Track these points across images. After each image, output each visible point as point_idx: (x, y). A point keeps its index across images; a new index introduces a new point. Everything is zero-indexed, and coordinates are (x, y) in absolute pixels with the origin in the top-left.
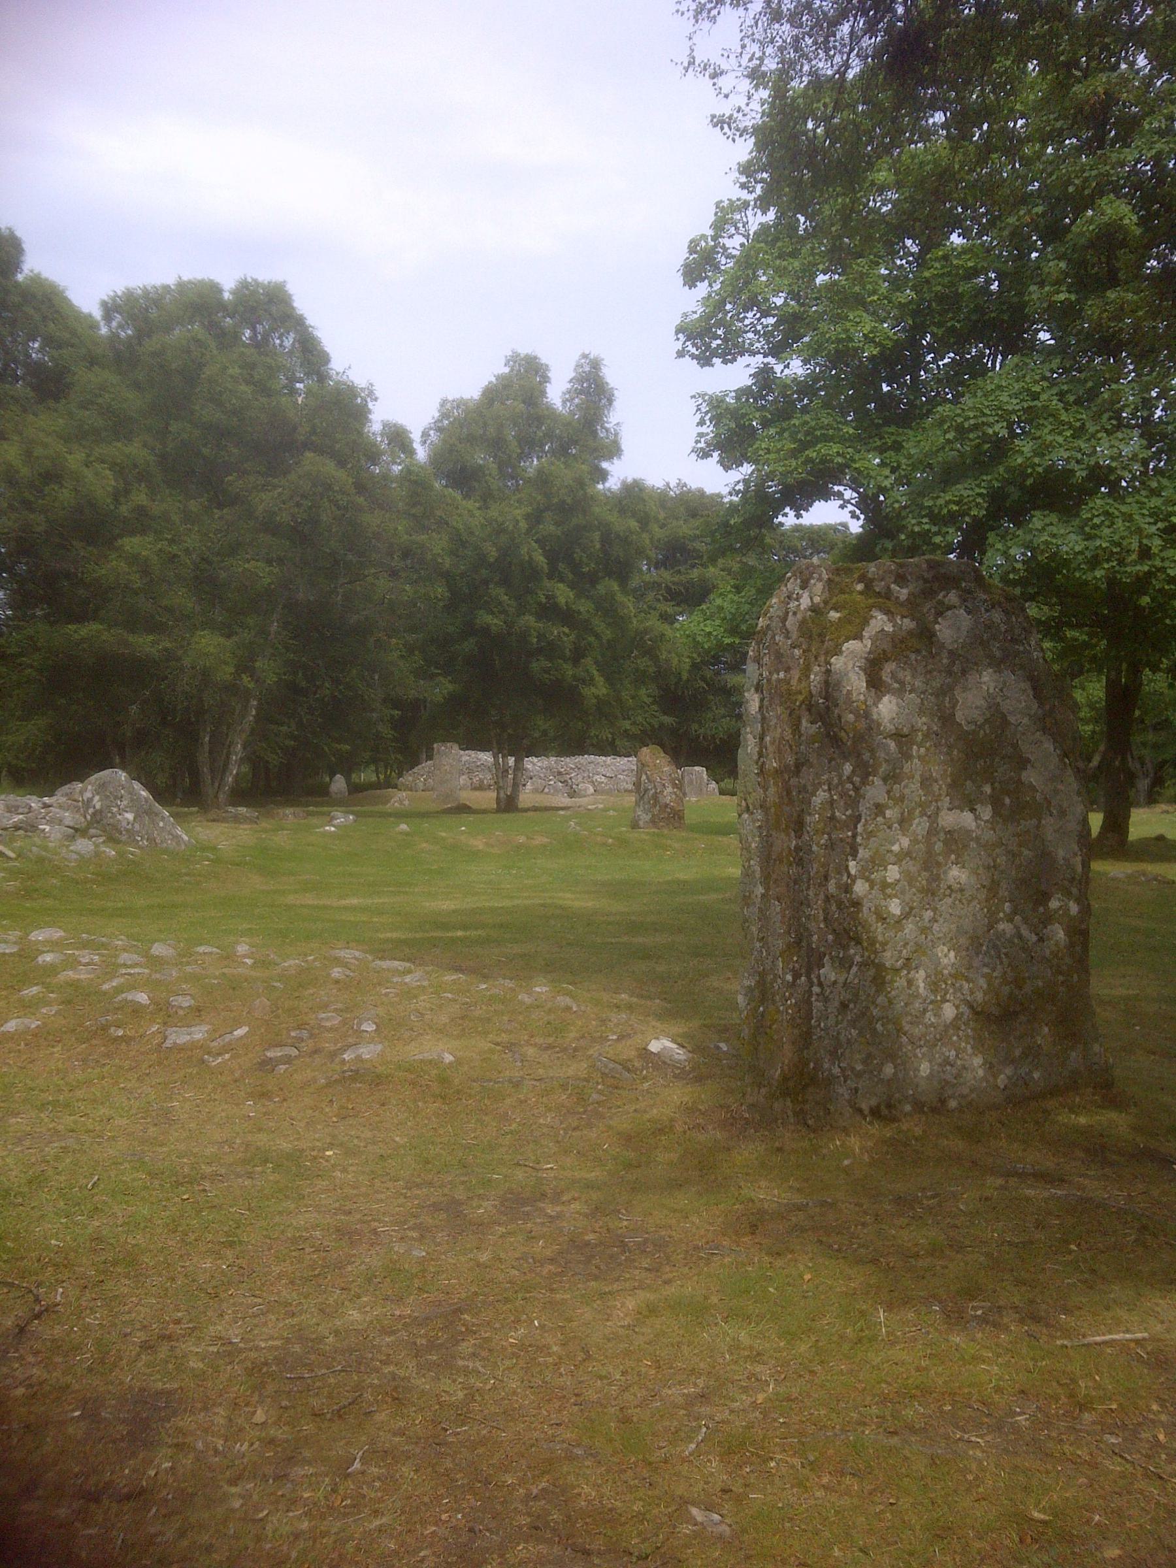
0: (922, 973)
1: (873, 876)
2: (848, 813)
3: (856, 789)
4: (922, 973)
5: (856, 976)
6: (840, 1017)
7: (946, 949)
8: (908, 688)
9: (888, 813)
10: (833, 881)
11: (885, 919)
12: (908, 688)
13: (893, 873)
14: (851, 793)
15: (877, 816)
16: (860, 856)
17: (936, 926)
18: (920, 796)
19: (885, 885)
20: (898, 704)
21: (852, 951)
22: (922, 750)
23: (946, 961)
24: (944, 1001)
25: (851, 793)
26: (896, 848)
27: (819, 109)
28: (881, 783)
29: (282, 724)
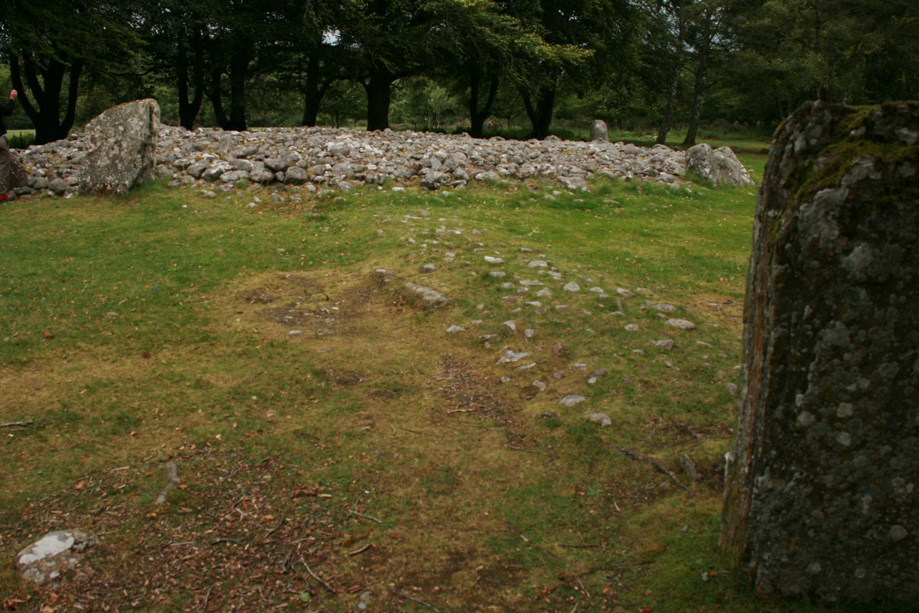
0: (867, 498)
1: (821, 410)
2: (804, 351)
3: (815, 330)
4: (867, 498)
5: (792, 489)
6: (773, 518)
7: (903, 481)
8: (889, 238)
9: (846, 356)
10: (781, 407)
11: (831, 448)
12: (889, 238)
13: (845, 410)
14: (810, 333)
15: (833, 357)
16: (808, 391)
17: (893, 461)
18: (892, 342)
19: (833, 419)
20: (873, 254)
21: (793, 468)
22: (903, 299)
23: (901, 491)
24: (893, 522)
25: (810, 333)
26: (852, 388)
27: (361, 28)
28: (844, 327)
29: (409, 219)
